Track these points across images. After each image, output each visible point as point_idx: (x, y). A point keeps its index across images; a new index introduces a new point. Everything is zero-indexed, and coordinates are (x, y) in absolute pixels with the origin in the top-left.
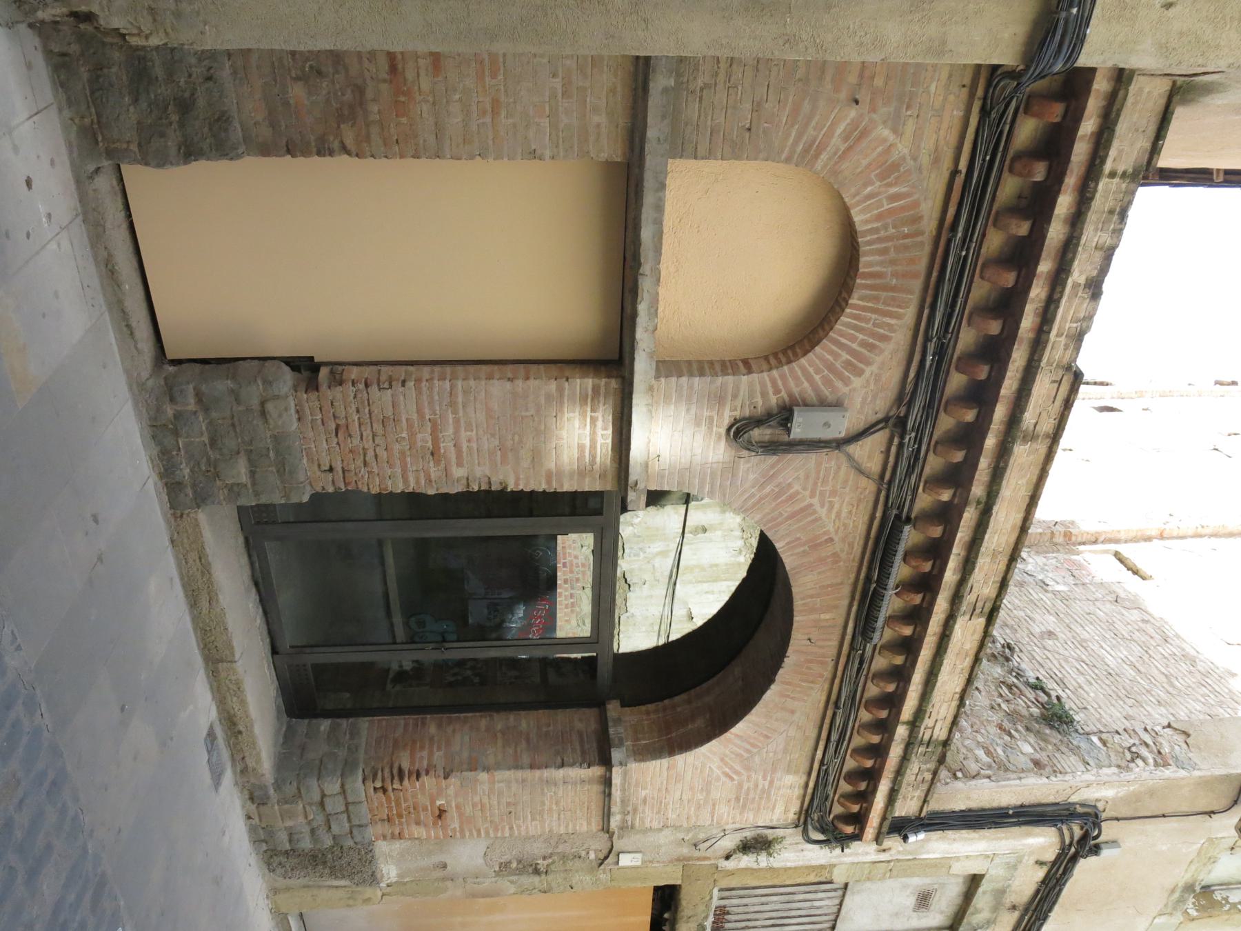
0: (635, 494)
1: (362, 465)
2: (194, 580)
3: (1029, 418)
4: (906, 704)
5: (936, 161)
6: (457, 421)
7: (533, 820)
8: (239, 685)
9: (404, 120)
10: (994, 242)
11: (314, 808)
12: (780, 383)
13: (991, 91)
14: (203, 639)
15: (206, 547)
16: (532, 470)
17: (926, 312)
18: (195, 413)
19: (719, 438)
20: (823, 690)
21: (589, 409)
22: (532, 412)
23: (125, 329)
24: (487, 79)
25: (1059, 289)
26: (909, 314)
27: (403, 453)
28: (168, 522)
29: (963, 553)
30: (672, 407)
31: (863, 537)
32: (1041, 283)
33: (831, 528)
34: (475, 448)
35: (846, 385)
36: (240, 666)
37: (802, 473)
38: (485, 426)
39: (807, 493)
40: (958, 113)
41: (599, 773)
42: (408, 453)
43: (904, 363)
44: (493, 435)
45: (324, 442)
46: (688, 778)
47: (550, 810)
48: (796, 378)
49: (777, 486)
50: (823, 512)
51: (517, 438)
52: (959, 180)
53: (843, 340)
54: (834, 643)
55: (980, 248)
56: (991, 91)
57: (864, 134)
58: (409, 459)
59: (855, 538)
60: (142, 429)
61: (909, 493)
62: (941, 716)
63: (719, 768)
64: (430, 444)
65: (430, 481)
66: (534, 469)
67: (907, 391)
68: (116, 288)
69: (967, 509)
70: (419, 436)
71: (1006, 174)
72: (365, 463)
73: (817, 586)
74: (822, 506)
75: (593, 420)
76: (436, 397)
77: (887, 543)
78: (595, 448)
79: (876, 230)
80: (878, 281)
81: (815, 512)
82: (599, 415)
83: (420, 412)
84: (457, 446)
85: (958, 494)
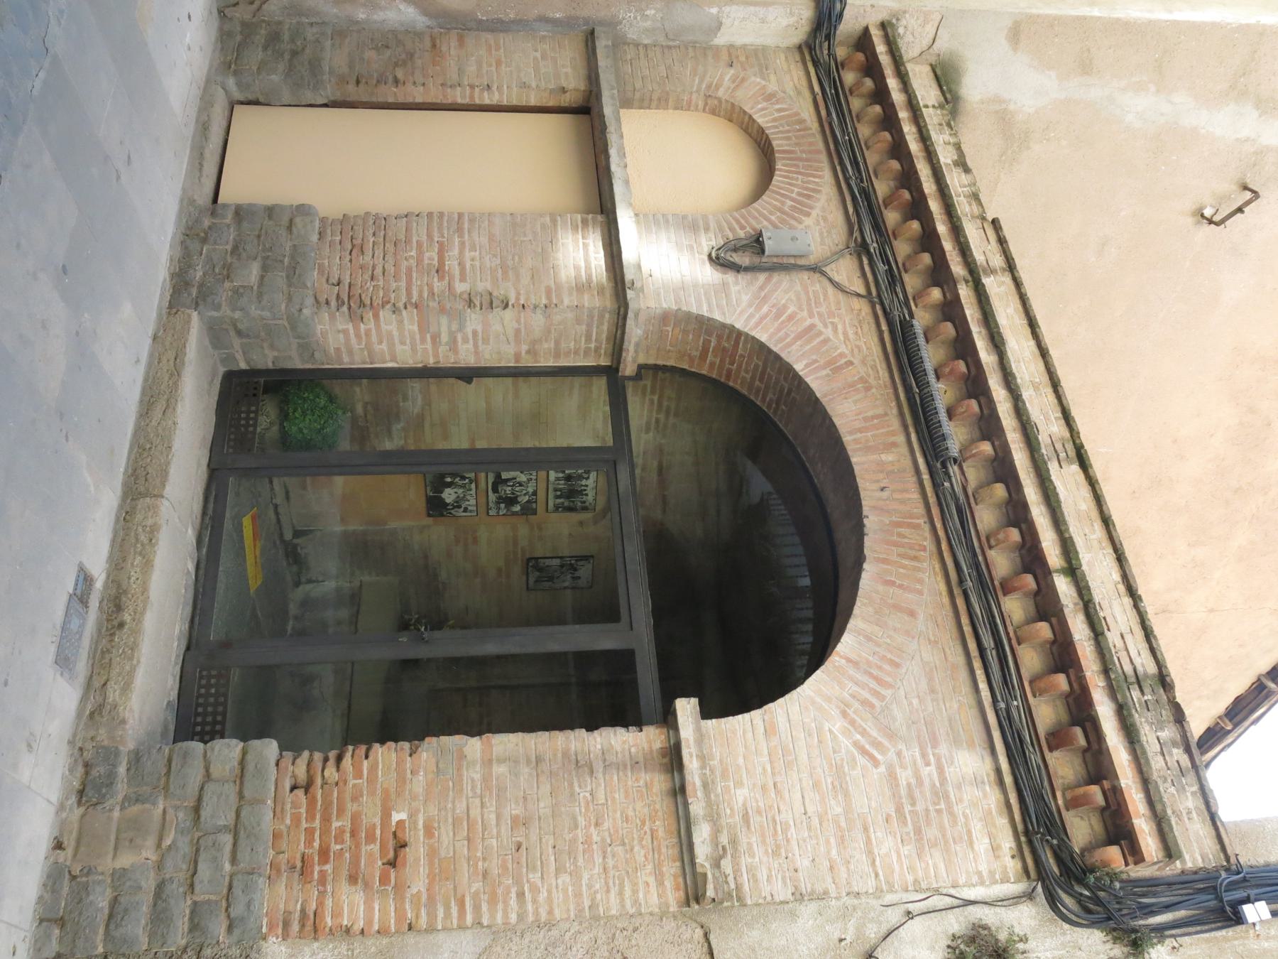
0: (632, 292)
1: (369, 279)
2: (158, 383)
3: (979, 257)
4: (1042, 538)
5: (799, 93)
6: (462, 244)
7: (558, 871)
8: (153, 531)
9: (438, 68)
10: (974, 474)
11: (181, 815)
12: (743, 222)
13: (1065, 911)
14: (136, 461)
15: (187, 345)
16: (532, 286)
17: (838, 168)
18: (228, 226)
19: (703, 263)
20: (935, 574)
21: (580, 237)
22: (530, 237)
23: (197, 164)
24: (493, 52)
25: (921, 121)
26: (827, 175)
27: (409, 270)
28: (159, 316)
29: (984, 331)
30: (654, 236)
31: (882, 358)
32: (907, 123)
33: (843, 349)
34: (478, 266)
35: (800, 223)
36: (164, 506)
37: (792, 295)
38: (488, 248)
39: (805, 313)
40: (802, 73)
41: (658, 745)
42: (414, 269)
43: (841, 208)
44: (495, 256)
45: (338, 258)
46: (803, 757)
47: (588, 841)
48: (755, 218)
49: (773, 307)
50: (829, 332)
51: (517, 258)
52: (820, 98)
53: (782, 191)
54: (915, 495)
55: (857, 136)
56: (1065, 911)
57: (743, 80)
58: (414, 275)
59: (874, 361)
60: (175, 234)
61: (905, 309)
62: (1125, 630)
63: (846, 732)
64: (435, 262)
65: (433, 294)
66: (534, 285)
67: (853, 221)
68: (204, 139)
69: (959, 287)
70: (427, 255)
71: (850, 98)
72: (372, 278)
73: (860, 417)
74: (826, 326)
75: (585, 246)
76: (445, 224)
77: (905, 341)
78: (590, 268)
79: (776, 127)
80: (792, 156)
81: (820, 333)
82: (590, 241)
83: (430, 236)
84: (462, 265)
85: (946, 290)
